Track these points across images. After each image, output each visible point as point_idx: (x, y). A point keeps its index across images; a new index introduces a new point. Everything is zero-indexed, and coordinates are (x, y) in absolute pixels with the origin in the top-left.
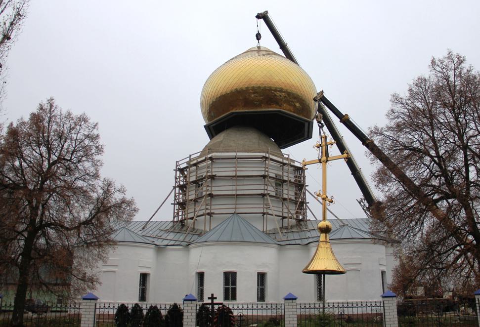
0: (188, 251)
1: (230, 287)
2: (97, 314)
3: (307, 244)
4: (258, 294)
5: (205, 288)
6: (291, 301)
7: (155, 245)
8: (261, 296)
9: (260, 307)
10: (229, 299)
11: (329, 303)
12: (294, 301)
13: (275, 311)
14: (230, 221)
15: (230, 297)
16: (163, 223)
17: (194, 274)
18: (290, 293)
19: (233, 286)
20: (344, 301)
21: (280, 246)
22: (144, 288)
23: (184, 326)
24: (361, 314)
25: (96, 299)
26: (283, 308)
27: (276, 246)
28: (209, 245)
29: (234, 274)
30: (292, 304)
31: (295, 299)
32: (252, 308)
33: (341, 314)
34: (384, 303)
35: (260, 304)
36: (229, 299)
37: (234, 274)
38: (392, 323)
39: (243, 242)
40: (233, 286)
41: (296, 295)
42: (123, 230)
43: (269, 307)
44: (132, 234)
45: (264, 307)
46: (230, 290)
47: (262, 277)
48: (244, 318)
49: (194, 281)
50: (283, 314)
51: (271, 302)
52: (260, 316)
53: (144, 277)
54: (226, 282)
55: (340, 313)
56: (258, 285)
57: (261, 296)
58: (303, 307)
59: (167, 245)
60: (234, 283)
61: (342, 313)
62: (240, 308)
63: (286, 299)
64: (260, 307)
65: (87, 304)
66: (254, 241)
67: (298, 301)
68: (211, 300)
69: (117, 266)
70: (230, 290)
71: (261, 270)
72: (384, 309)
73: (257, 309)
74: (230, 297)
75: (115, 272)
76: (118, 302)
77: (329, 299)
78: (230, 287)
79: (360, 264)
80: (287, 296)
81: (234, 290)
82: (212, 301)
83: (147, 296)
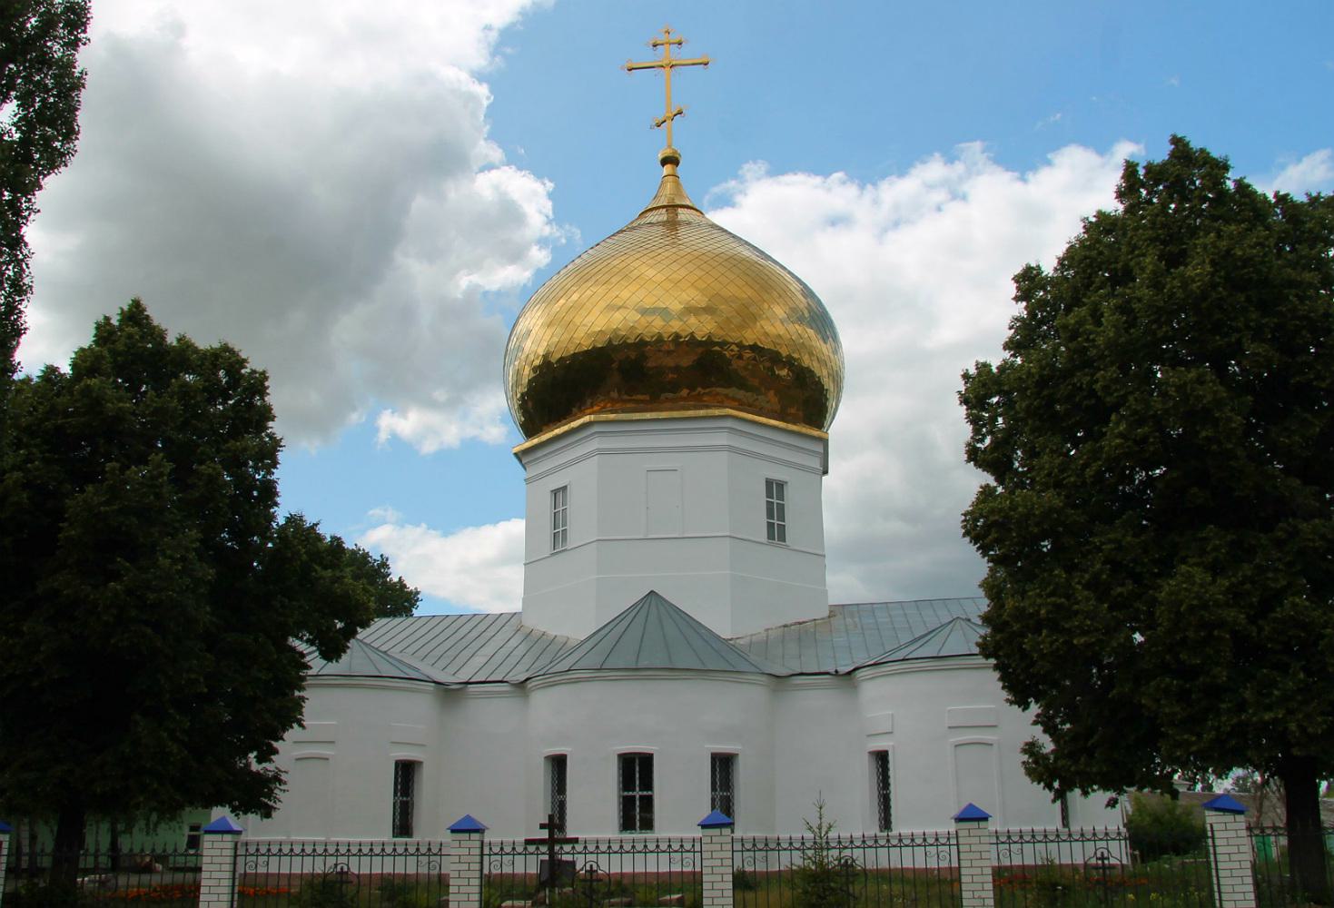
0: (854, 687)
1: (637, 793)
2: (241, 875)
3: (849, 673)
4: (394, 821)
5: (568, 799)
6: (975, 824)
7: (434, 682)
8: (403, 825)
9: (400, 850)
10: (635, 829)
11: (247, 844)
12: (982, 824)
13: (424, 860)
14: (641, 608)
15: (638, 824)
16: (425, 620)
17: (541, 761)
18: (971, 805)
19: (645, 793)
20: (758, 835)
21: (774, 679)
22: (407, 802)
23: (201, 904)
24: (1019, 866)
25: (480, 831)
26: (697, 848)
27: (764, 678)
28: (577, 681)
29: (646, 761)
30: (979, 832)
31: (985, 819)
32: (383, 853)
33: (342, 873)
34: (957, 837)
35: (401, 844)
36: (635, 829)
37: (646, 761)
38: (979, 887)
39: (672, 671)
40: (645, 793)
41: (983, 806)
42: (958, 624)
43: (664, 846)
44: (366, 649)
45: (412, 850)
46: (638, 803)
47: (723, 766)
48: (351, 878)
49: (541, 778)
50: (955, 864)
51: (750, 835)
52: (908, 869)
53: (406, 773)
54: (627, 781)
55: (339, 869)
56: (714, 789)
57: (403, 825)
58: (749, 846)
59: (468, 683)
60: (647, 783)
61: (345, 869)
62: (377, 852)
63: (959, 819)
64: (400, 850)
65: (216, 845)
66: (724, 666)
67: (992, 826)
68: (547, 831)
69: (333, 742)
70: (638, 803)
71: (724, 748)
72: (959, 852)
73: (395, 853)
74: (638, 824)
75: (327, 759)
76: (333, 839)
77: (207, 837)
78: (637, 793)
79: (333, 742)
80: (460, 822)
81: (648, 803)
82: (551, 834)
83: (414, 824)
